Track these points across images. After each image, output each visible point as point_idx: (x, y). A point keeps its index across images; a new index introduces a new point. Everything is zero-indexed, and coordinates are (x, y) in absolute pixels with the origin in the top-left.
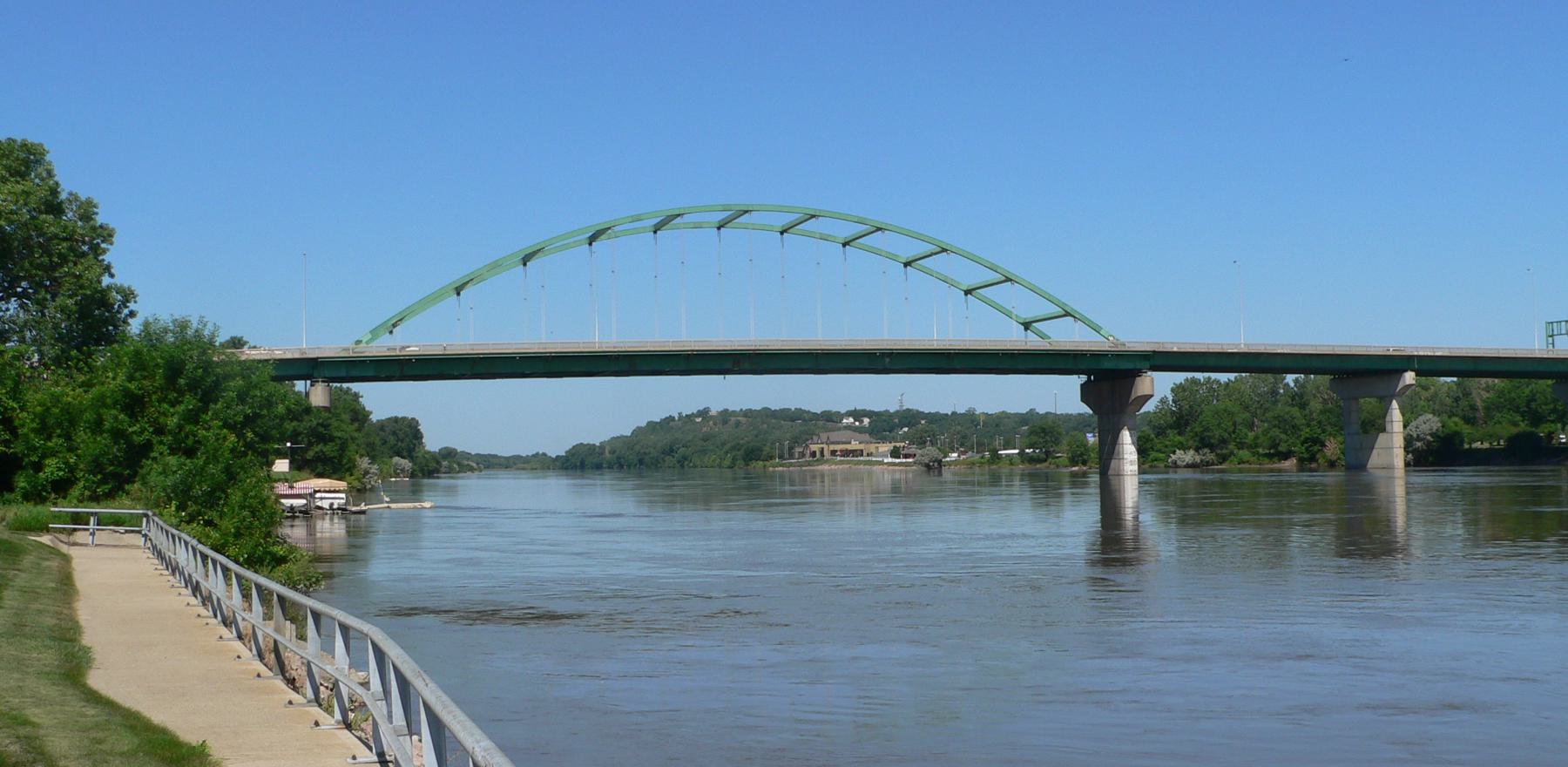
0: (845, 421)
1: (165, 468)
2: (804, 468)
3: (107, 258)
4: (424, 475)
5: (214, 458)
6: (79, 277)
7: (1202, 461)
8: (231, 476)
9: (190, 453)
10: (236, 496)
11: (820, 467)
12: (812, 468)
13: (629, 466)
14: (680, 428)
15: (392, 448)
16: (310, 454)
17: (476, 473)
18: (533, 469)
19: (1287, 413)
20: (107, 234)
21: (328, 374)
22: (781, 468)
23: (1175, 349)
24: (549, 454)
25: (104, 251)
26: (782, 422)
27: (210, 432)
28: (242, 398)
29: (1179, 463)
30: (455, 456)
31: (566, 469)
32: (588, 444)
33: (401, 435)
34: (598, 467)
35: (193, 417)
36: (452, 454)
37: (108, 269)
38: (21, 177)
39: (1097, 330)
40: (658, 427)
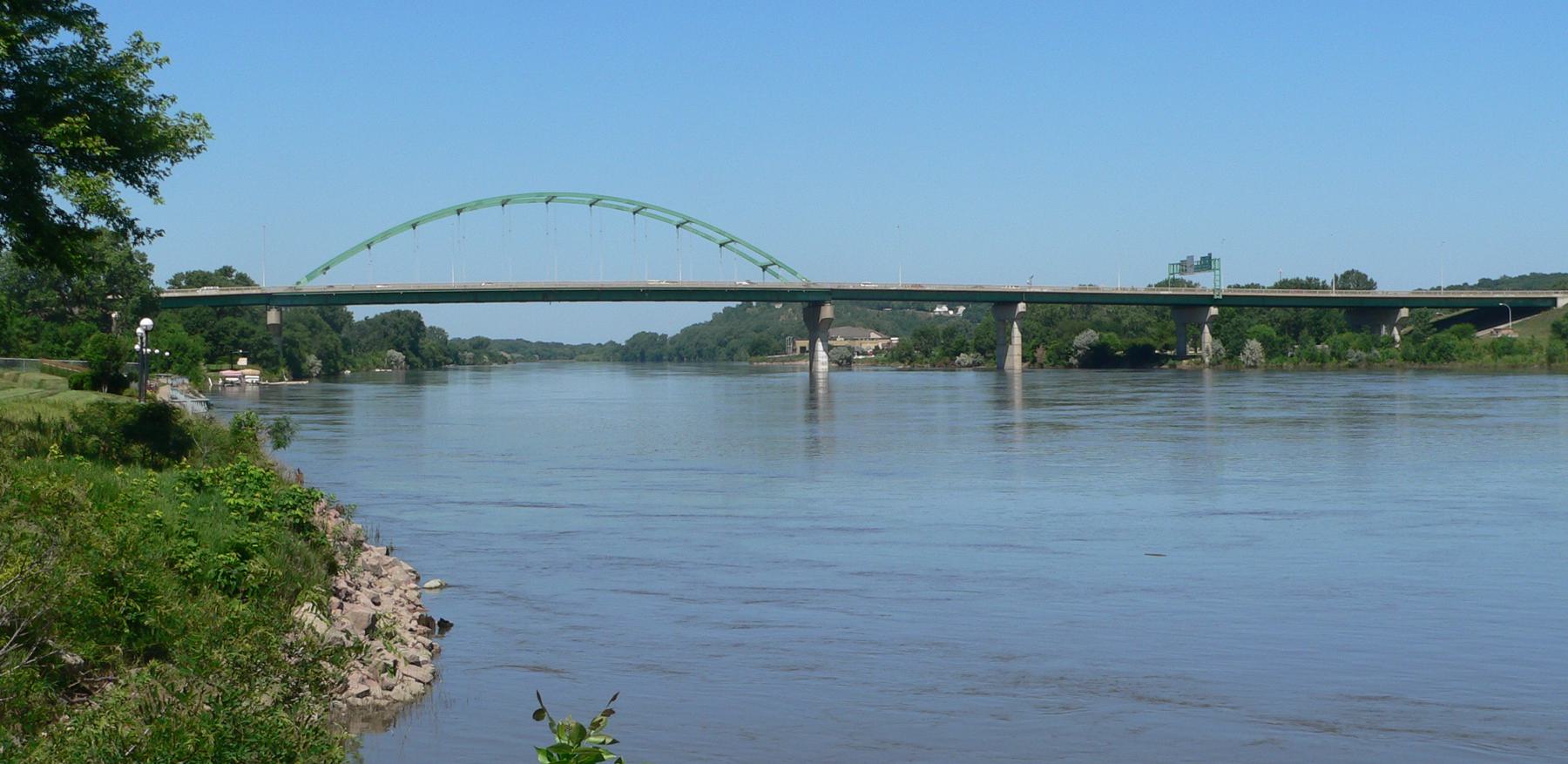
0: (937, 309)
1: (176, 366)
2: (786, 363)
3: (152, 278)
4: (428, 367)
5: (186, 365)
6: (141, 288)
7: (974, 362)
8: (190, 368)
9: (181, 363)
10: (190, 373)
11: (800, 363)
12: (793, 363)
13: (689, 358)
14: (757, 316)
15: (392, 341)
16: (259, 355)
17: (510, 365)
18: (594, 360)
19: (1028, 326)
20: (151, 267)
21: (279, 303)
22: (764, 363)
23: (851, 287)
24: (618, 342)
25: (150, 275)
26: (869, 310)
27: (186, 359)
28: (193, 351)
29: (963, 364)
30: (487, 346)
31: (627, 360)
32: (650, 333)
33: (401, 328)
34: (658, 359)
35: (182, 355)
36: (484, 344)
37: (152, 281)
38: (253, 513)
39: (794, 273)
40: (733, 314)
